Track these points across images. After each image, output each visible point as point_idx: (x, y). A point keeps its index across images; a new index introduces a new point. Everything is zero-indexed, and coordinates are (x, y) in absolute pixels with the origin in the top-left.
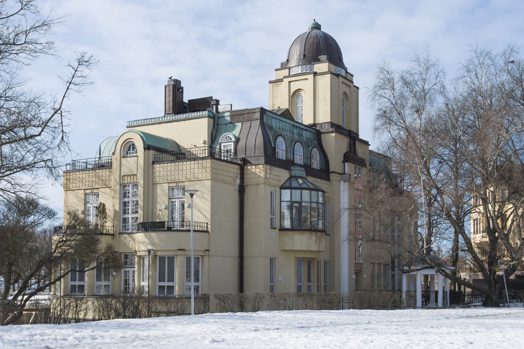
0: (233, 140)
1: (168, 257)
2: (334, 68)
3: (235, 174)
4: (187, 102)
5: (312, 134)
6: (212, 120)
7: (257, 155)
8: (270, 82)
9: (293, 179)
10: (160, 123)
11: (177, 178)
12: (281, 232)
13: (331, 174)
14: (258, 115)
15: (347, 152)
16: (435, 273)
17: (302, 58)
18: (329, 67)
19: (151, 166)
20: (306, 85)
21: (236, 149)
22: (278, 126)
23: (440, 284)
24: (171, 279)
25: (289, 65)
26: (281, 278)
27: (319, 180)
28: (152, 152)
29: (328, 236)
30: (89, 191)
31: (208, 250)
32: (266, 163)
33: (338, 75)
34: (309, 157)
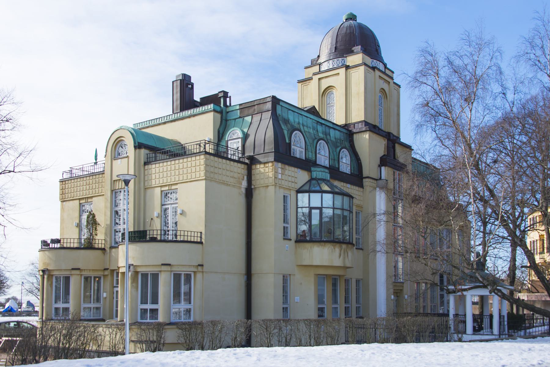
2: (369, 61)
3: (239, 175)
4: (199, 100)
5: (342, 134)
6: (219, 116)
7: (267, 151)
8: (299, 82)
9: (314, 182)
10: (165, 123)
12: (297, 244)
13: (364, 180)
14: (269, 106)
15: (384, 155)
16: (488, 293)
17: (334, 51)
18: (363, 59)
20: (337, 81)
21: (243, 146)
22: (297, 120)
23: (496, 306)
24: (155, 301)
25: (319, 61)
26: (297, 299)
27: (349, 186)
28: (143, 151)
29: (361, 251)
30: (84, 201)
31: (202, 265)
32: (277, 160)
33: (374, 68)
34: (335, 158)
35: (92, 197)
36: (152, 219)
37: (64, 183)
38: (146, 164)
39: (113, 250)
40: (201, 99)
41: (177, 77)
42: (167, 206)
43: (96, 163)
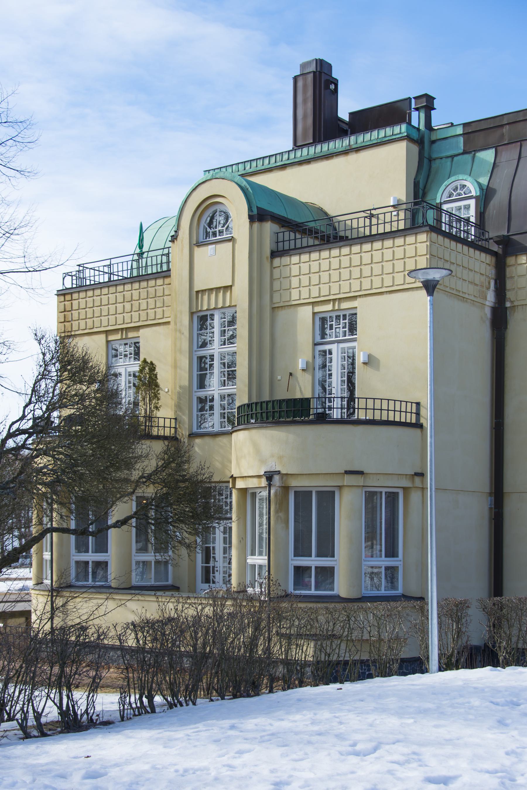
0: (473, 193)
1: (318, 492)
3: (483, 278)
10: (283, 167)
11: (335, 289)
19: (267, 265)
21: (481, 215)
24: (327, 548)
28: (269, 227)
35: (137, 328)
36: (291, 374)
37: (68, 297)
38: (274, 254)
39: (198, 441)
40: (351, 114)
41: (303, 66)
42: (327, 347)
43: (141, 255)
